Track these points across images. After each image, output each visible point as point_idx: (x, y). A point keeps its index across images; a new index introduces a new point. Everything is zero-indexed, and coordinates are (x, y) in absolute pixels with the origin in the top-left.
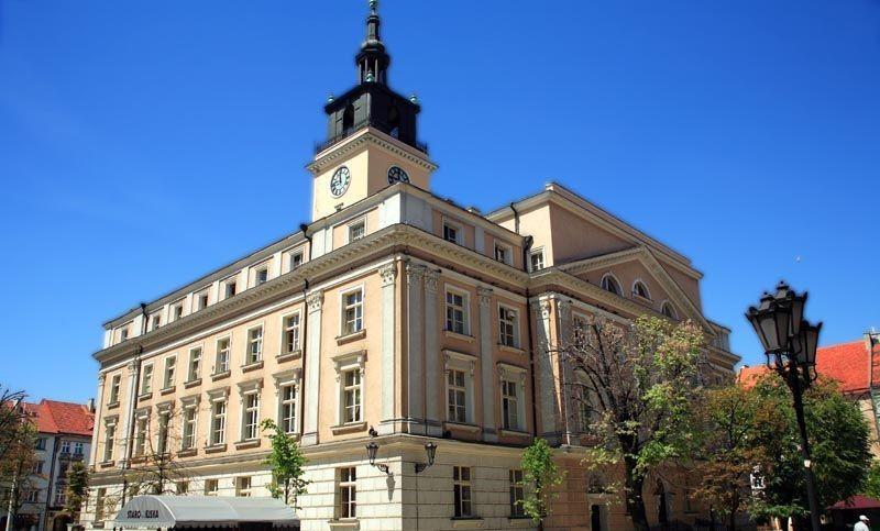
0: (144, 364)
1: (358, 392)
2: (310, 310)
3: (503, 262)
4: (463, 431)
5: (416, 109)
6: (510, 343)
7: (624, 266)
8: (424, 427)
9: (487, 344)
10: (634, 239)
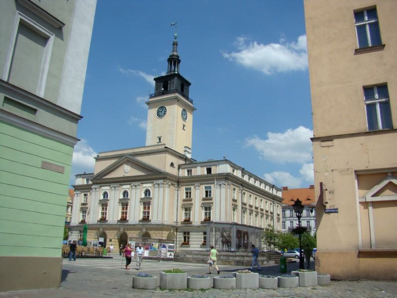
5: (190, 84)
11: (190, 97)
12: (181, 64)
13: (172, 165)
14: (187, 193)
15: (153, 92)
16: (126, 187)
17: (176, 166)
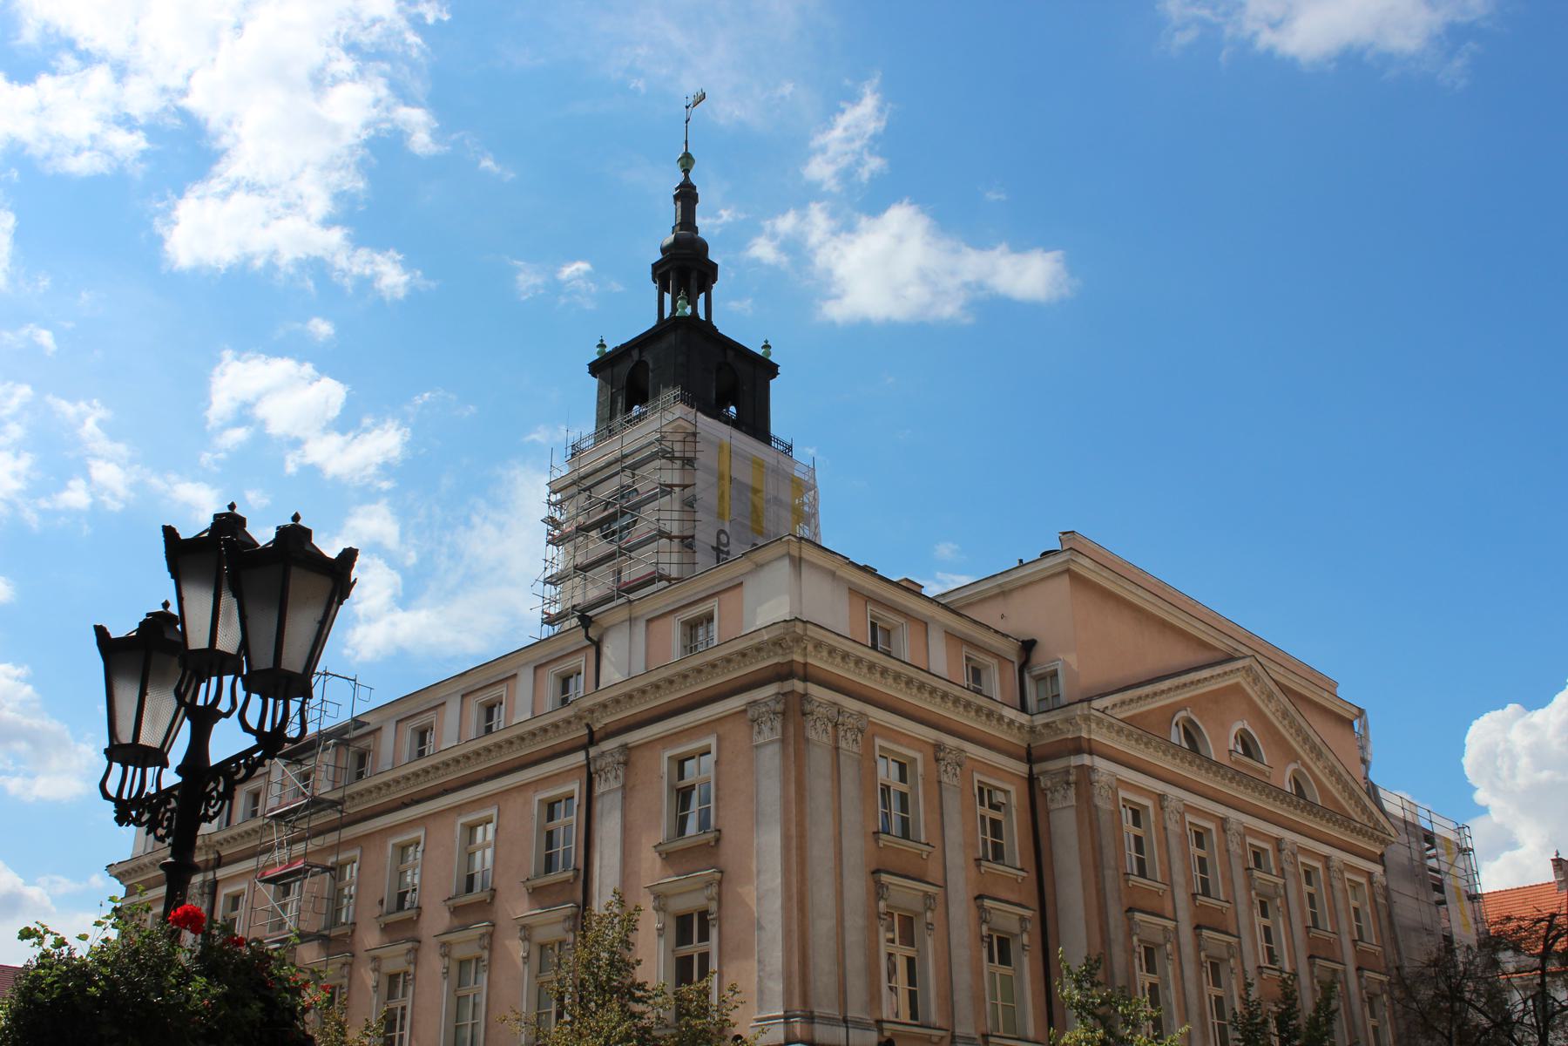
0: (223, 892)
1: (704, 957)
2: (599, 788)
3: (888, 654)
4: (1032, 982)
5: (772, 370)
6: (998, 854)
7: (1215, 697)
8: (842, 1031)
9: (957, 859)
10: (1235, 645)
11: (774, 430)
12: (716, 289)
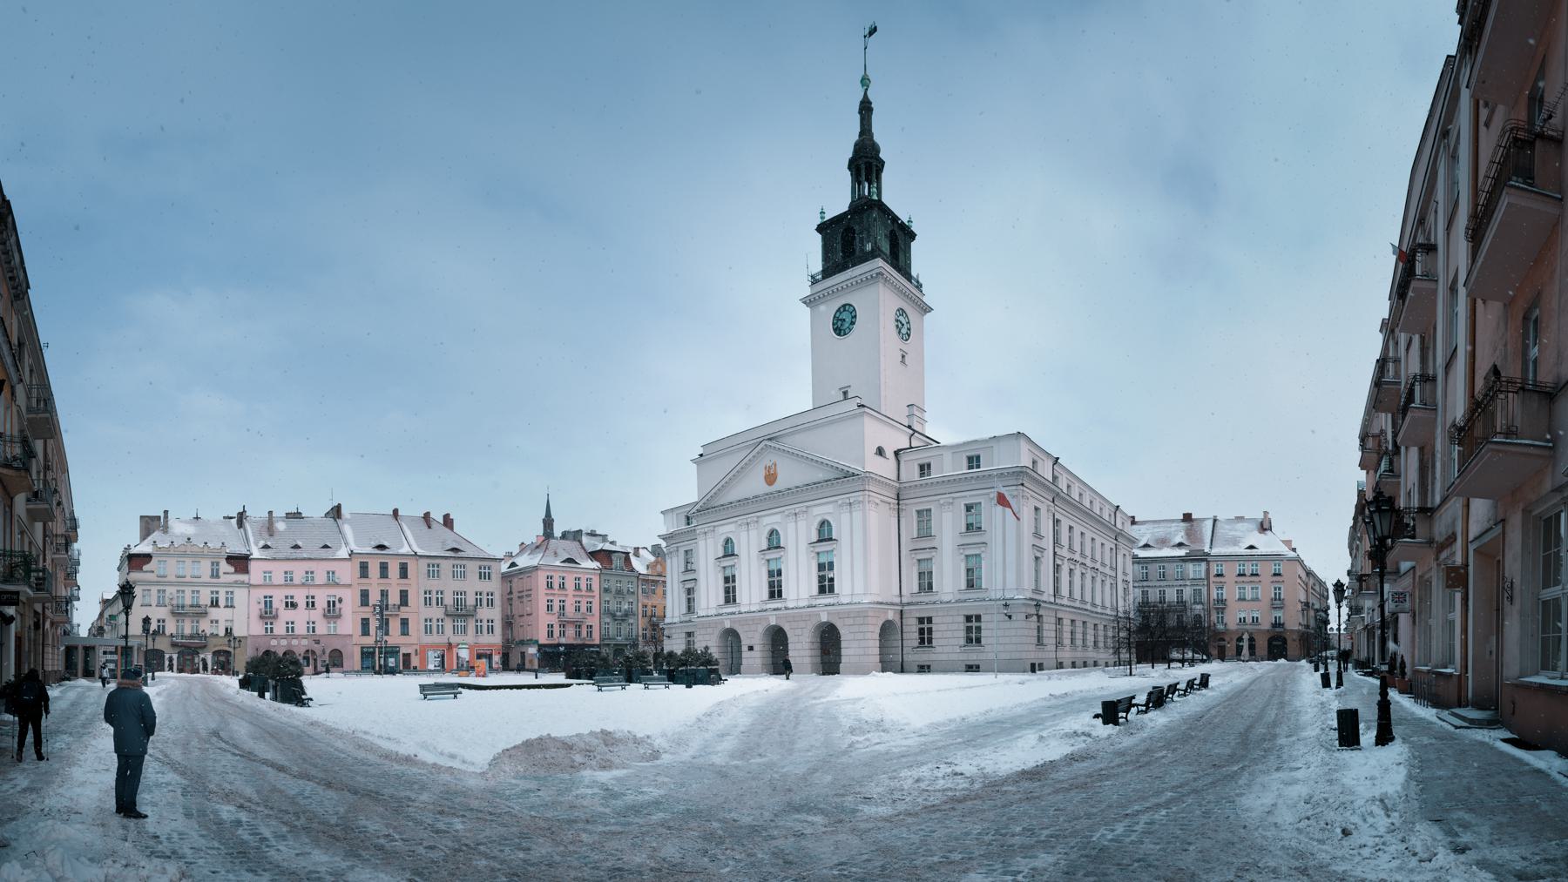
5: (912, 236)
13: (880, 452)
14: (921, 631)
15: (817, 266)
16: (771, 520)
17: (890, 453)
